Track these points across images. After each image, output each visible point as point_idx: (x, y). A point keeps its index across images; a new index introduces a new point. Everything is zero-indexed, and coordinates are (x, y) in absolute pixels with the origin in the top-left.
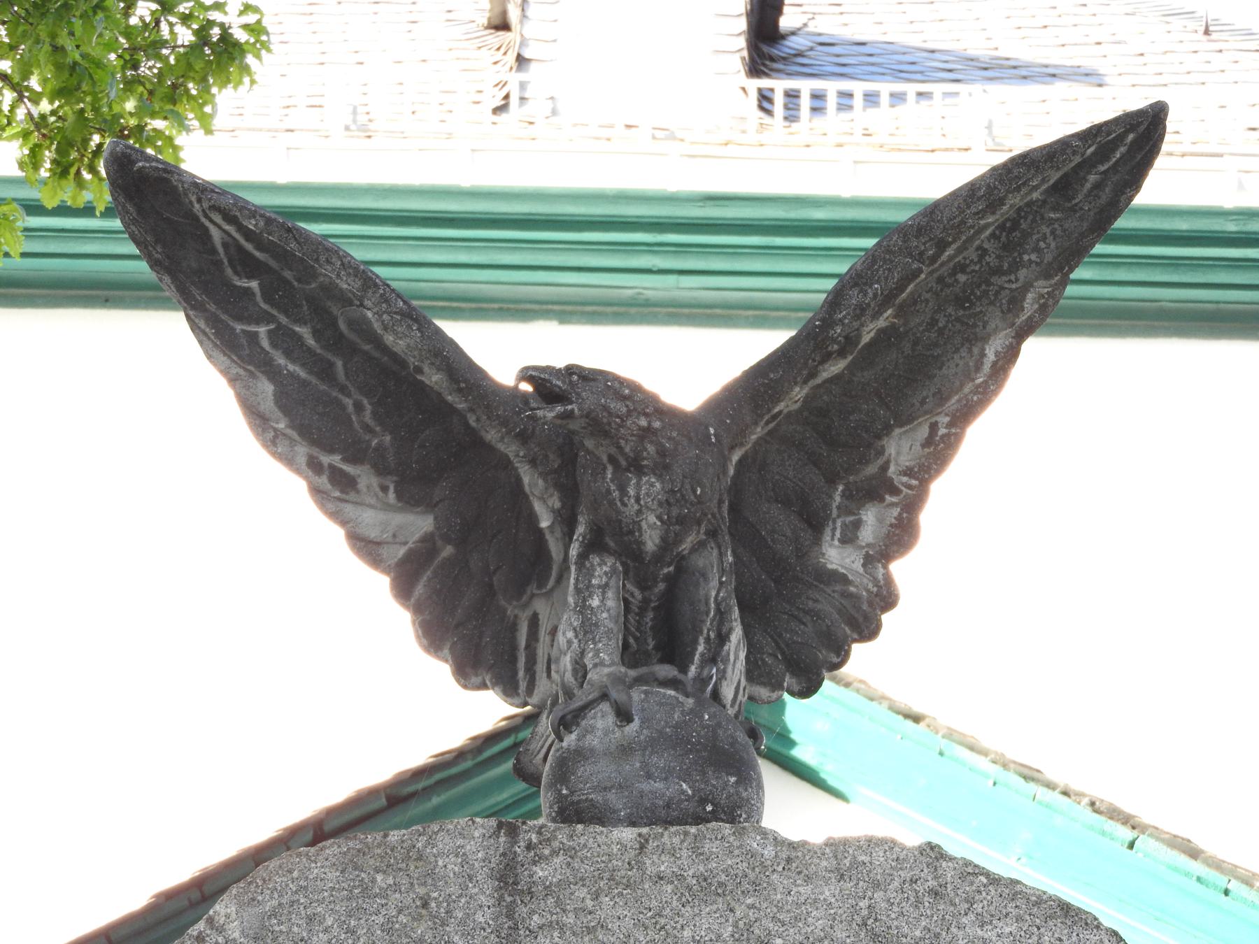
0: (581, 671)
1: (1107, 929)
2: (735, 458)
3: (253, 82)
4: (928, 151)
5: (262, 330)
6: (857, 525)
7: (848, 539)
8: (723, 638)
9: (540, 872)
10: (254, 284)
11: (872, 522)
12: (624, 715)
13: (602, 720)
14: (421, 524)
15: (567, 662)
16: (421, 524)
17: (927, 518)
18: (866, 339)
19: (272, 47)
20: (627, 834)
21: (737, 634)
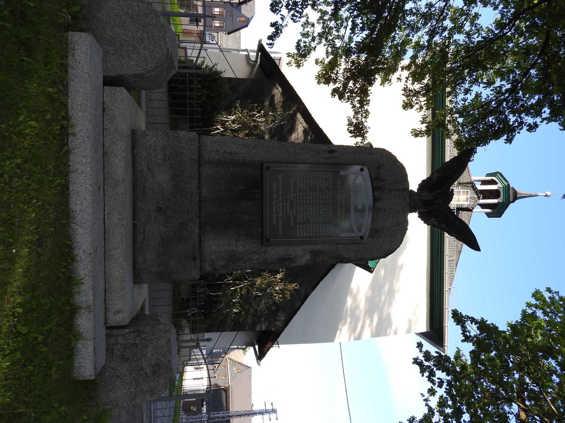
0: (422, 196)
1: (335, 265)
2: (443, 210)
3: (384, 87)
4: (531, 196)
5: (455, 164)
6: (436, 221)
7: (434, 221)
8: (425, 209)
9: (405, 193)
10: (460, 162)
11: (436, 223)
12: (419, 200)
13: (418, 198)
14: (435, 180)
15: (423, 194)
16: (435, 180)
17: (516, 201)
18: (456, 222)
19: (386, 84)
20: (408, 201)
21: (425, 210)
